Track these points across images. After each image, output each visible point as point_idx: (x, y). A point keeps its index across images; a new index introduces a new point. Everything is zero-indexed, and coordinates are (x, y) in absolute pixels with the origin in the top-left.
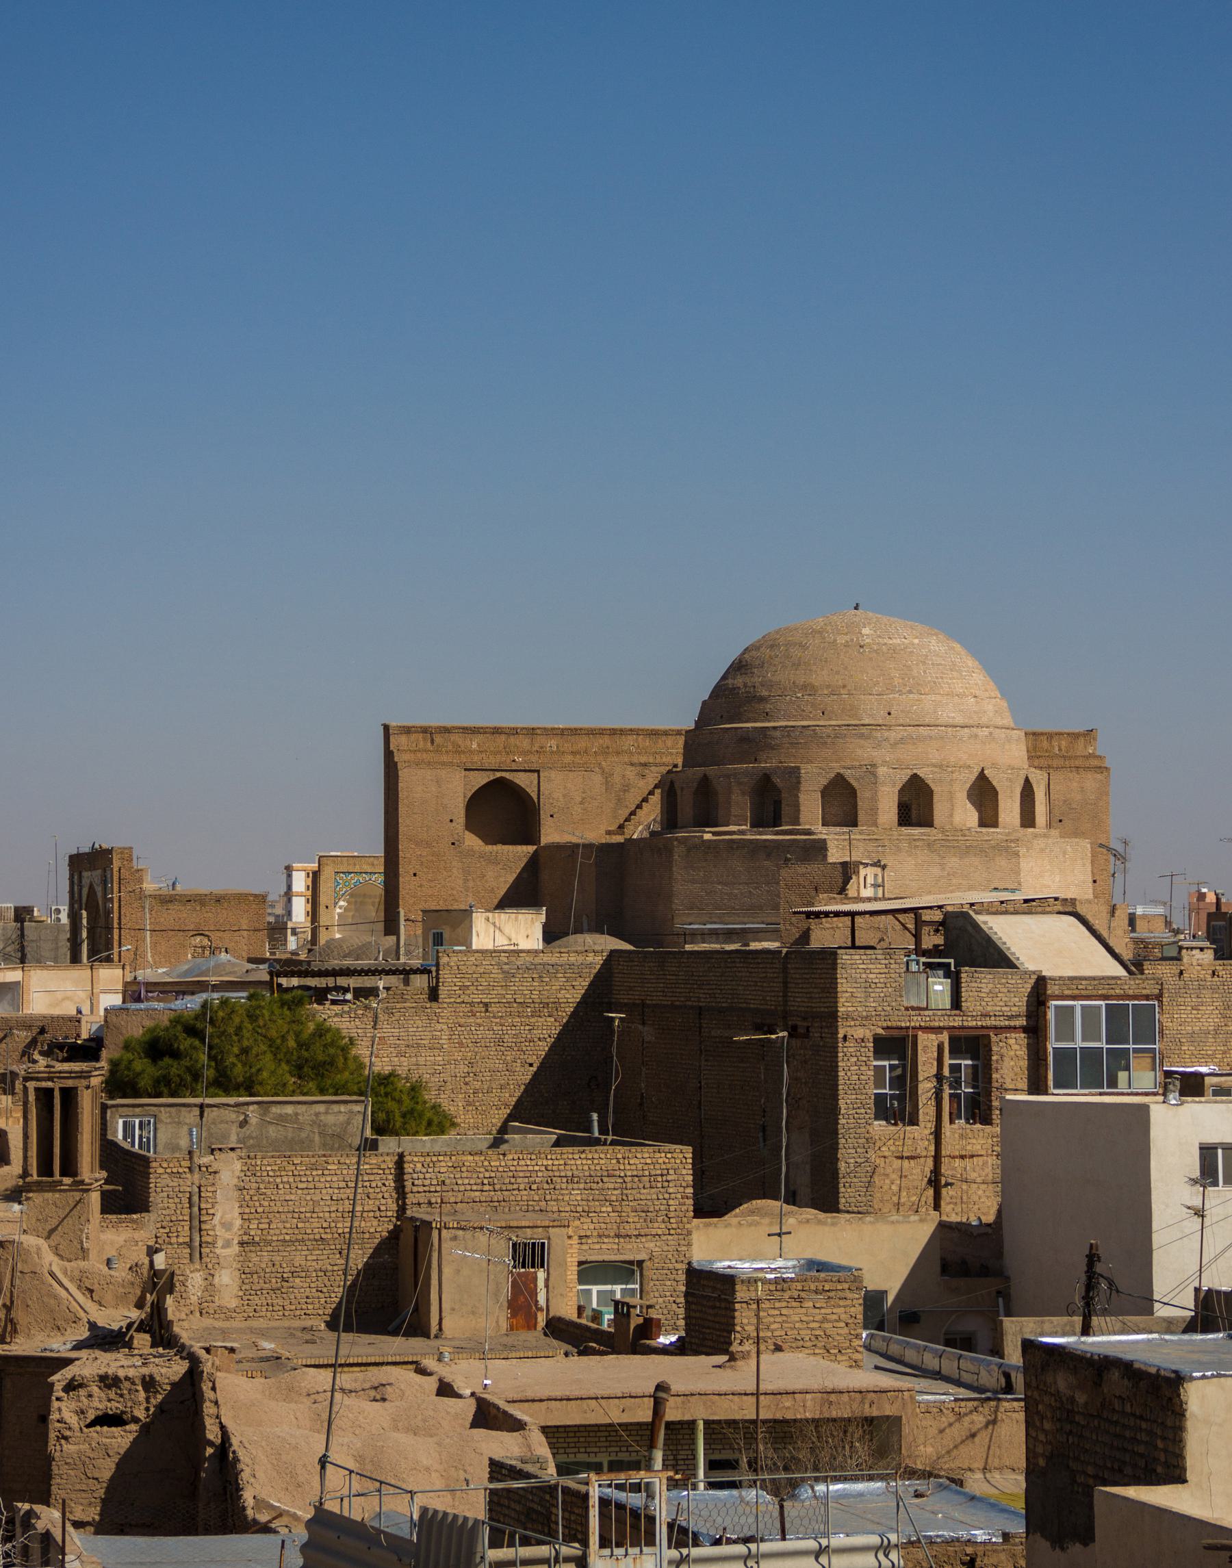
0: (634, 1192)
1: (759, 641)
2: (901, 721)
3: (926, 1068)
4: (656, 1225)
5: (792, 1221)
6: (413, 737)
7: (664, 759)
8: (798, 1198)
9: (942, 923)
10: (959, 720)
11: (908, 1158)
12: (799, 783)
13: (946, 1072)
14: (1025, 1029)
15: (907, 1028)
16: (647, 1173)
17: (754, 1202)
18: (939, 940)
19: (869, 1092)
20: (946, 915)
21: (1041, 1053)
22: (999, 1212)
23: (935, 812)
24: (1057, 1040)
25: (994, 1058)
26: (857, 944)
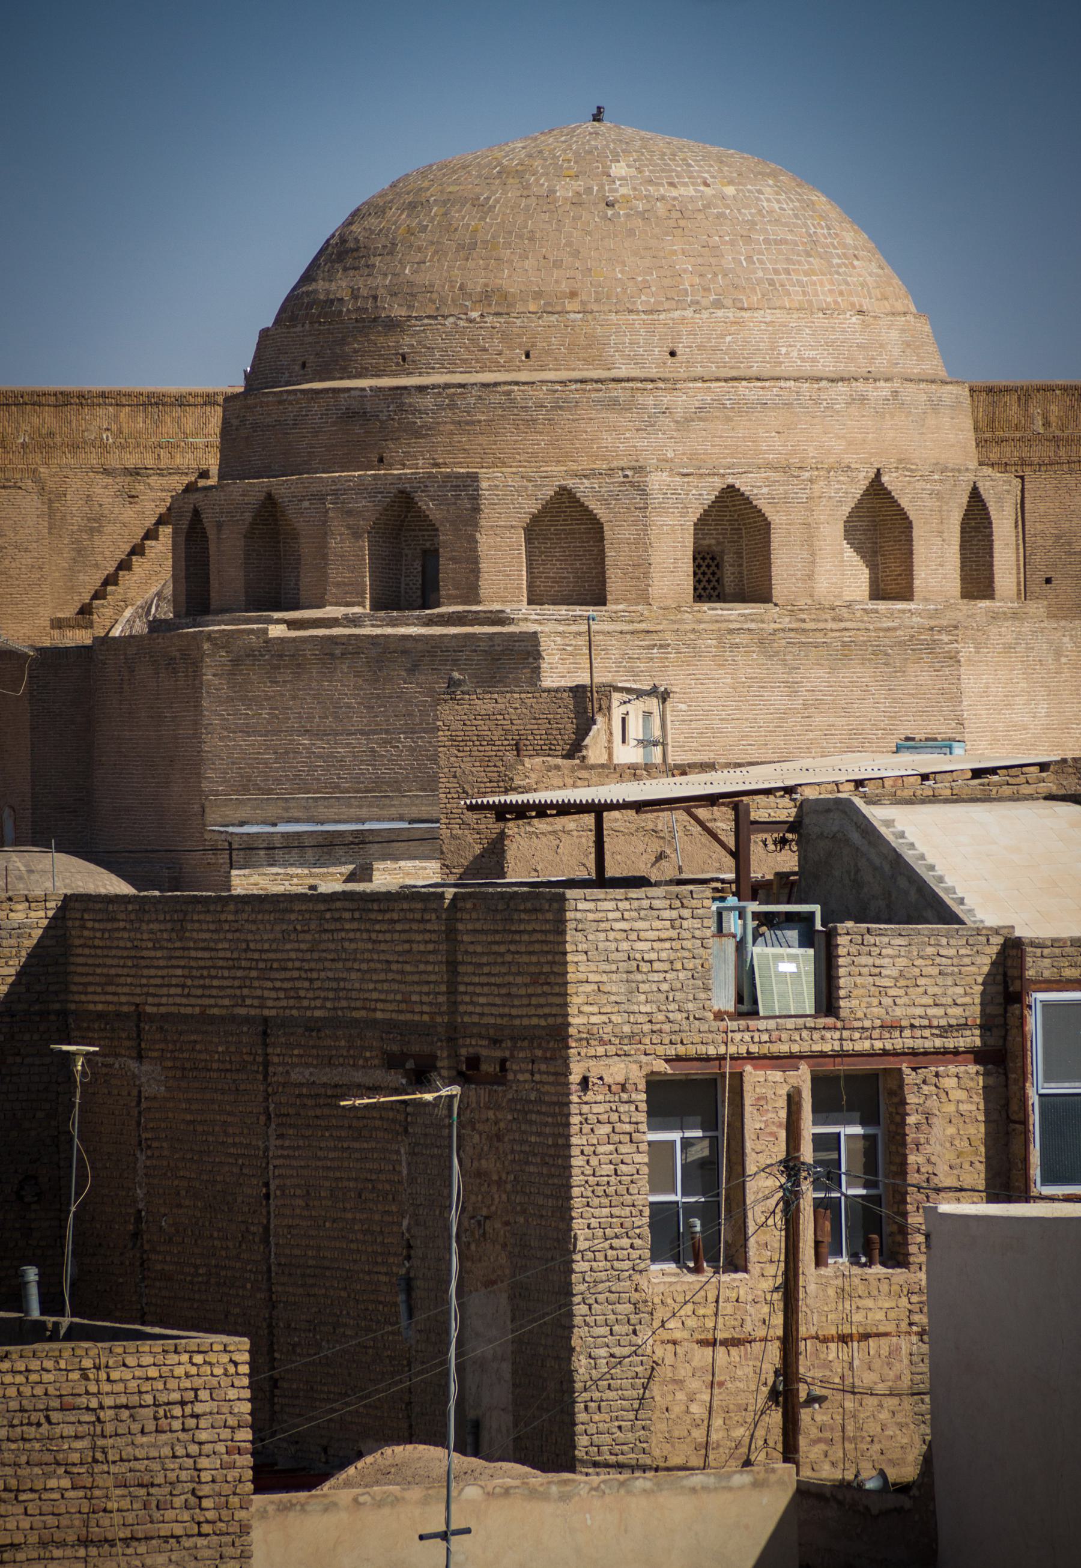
0: (120, 1442)
1: (382, 195)
2: (699, 371)
3: (763, 1146)
4: (170, 1514)
5: (472, 1492)
7: (178, 460)
8: (485, 1436)
9: (794, 826)
10: (827, 365)
11: (725, 1343)
12: (477, 510)
13: (807, 1153)
14: (979, 1056)
15: (721, 1058)
16: (148, 1399)
17: (388, 1451)
18: (788, 861)
19: (640, 1200)
20: (803, 807)
21: (1014, 1106)
22: (928, 1460)
23: (775, 570)
24: (1048, 1078)
25: (911, 1120)
26: (611, 872)
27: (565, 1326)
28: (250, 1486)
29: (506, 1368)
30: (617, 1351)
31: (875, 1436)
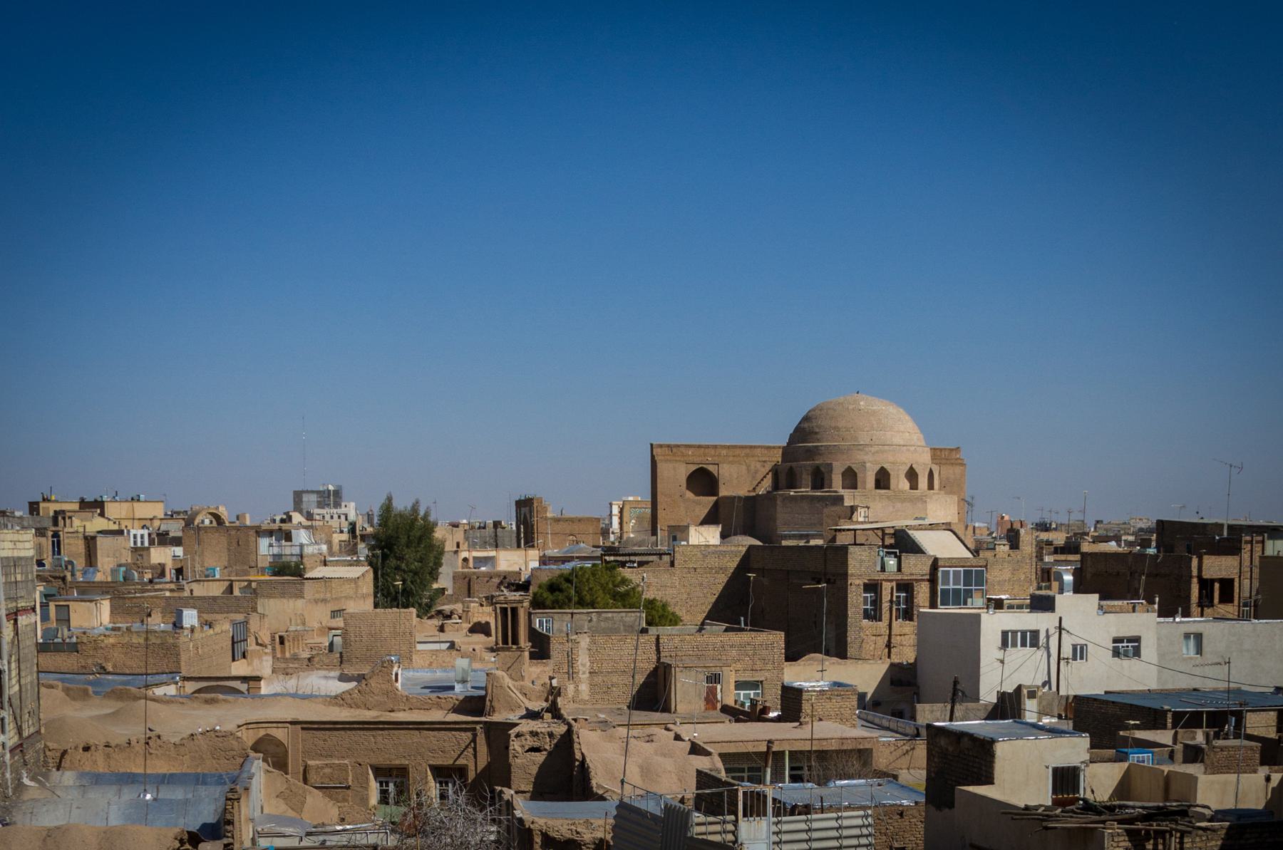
3: (886, 597)
18: (892, 541)
31: (906, 654)
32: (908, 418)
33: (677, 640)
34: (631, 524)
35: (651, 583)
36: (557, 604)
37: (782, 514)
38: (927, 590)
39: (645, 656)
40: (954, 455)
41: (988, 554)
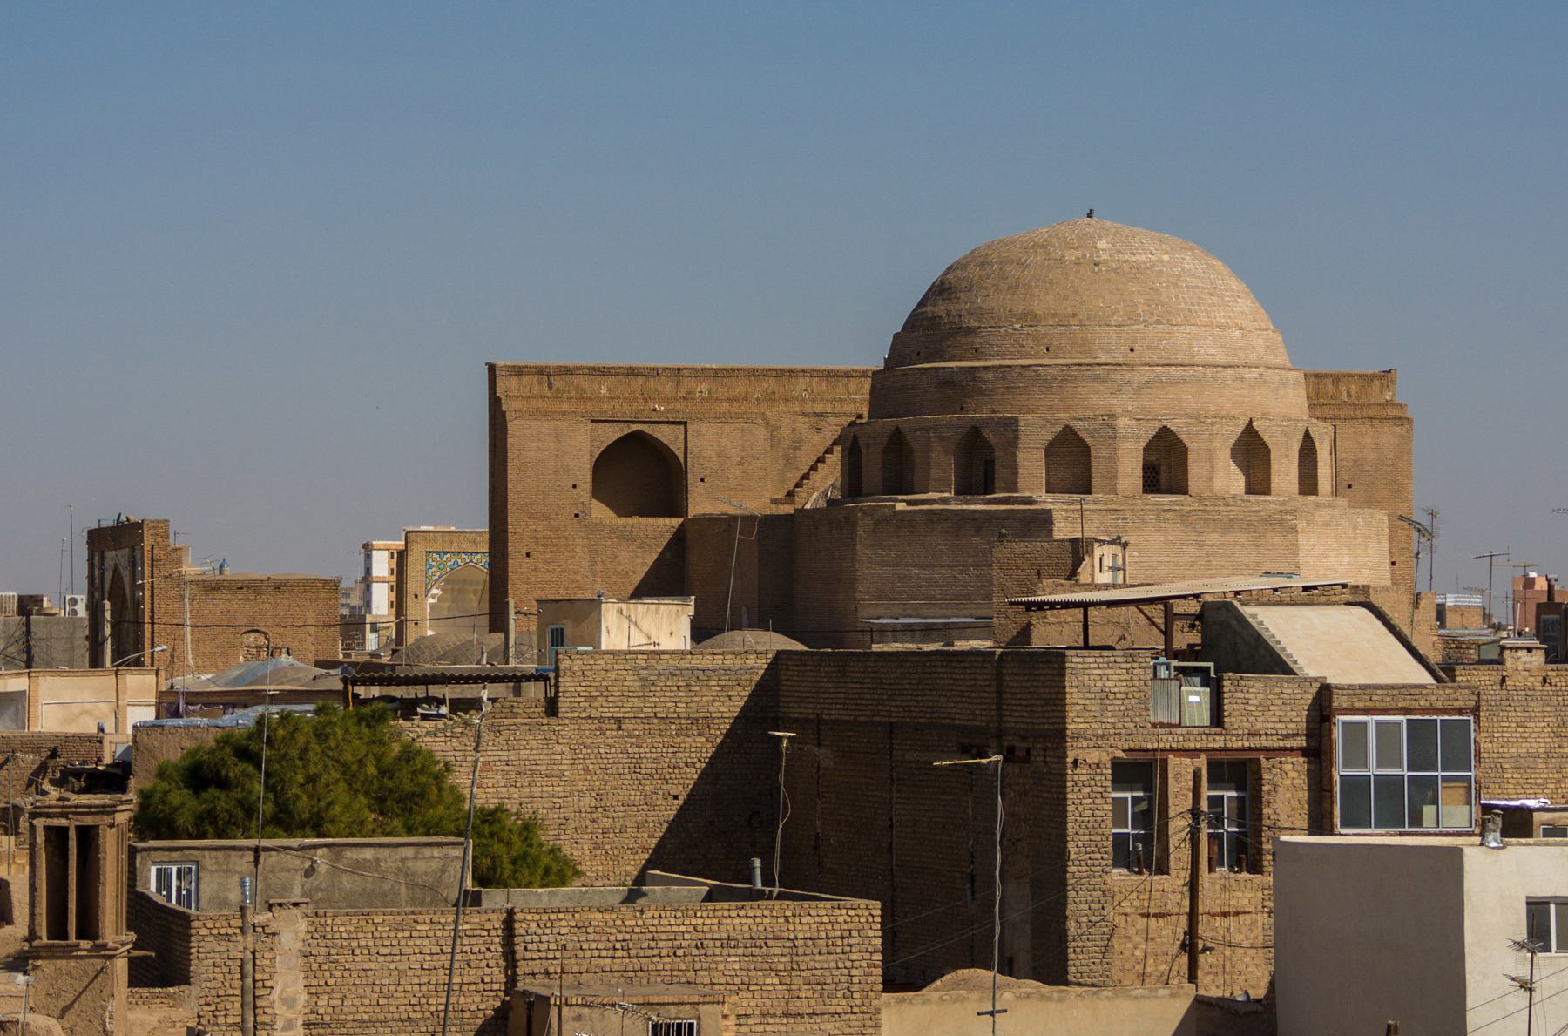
0: (807, 959)
2: (1147, 360)
4: (835, 1001)
5: (1008, 996)
6: (526, 379)
7: (845, 408)
9: (1199, 617)
10: (1221, 358)
11: (1155, 915)
12: (1017, 438)
13: (1204, 806)
14: (1304, 752)
15: (1155, 750)
16: (823, 935)
17: (960, 972)
18: (1195, 638)
19: (1107, 831)
20: (1204, 606)
21: (1325, 782)
22: (1272, 984)
23: (1190, 476)
25: (1265, 788)
26: (1091, 643)
27: (1063, 904)
28: (880, 987)
29: (1028, 927)
30: (1093, 918)
31: (1243, 973)
32: (1236, 285)
33: (565, 924)
34: (428, 601)
35: (490, 764)
36: (211, 825)
37: (872, 566)
38: (1302, 781)
39: (472, 975)
40: (1375, 393)
41: (1483, 678)
